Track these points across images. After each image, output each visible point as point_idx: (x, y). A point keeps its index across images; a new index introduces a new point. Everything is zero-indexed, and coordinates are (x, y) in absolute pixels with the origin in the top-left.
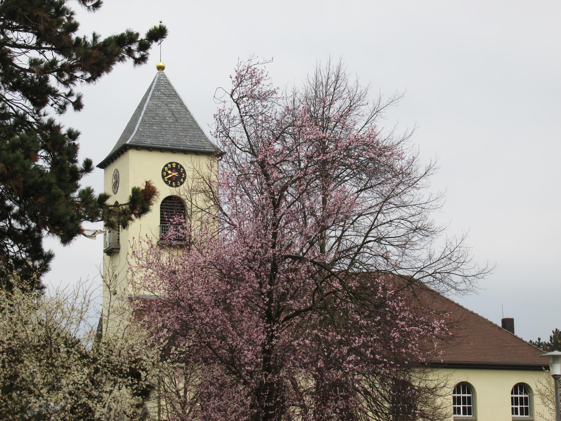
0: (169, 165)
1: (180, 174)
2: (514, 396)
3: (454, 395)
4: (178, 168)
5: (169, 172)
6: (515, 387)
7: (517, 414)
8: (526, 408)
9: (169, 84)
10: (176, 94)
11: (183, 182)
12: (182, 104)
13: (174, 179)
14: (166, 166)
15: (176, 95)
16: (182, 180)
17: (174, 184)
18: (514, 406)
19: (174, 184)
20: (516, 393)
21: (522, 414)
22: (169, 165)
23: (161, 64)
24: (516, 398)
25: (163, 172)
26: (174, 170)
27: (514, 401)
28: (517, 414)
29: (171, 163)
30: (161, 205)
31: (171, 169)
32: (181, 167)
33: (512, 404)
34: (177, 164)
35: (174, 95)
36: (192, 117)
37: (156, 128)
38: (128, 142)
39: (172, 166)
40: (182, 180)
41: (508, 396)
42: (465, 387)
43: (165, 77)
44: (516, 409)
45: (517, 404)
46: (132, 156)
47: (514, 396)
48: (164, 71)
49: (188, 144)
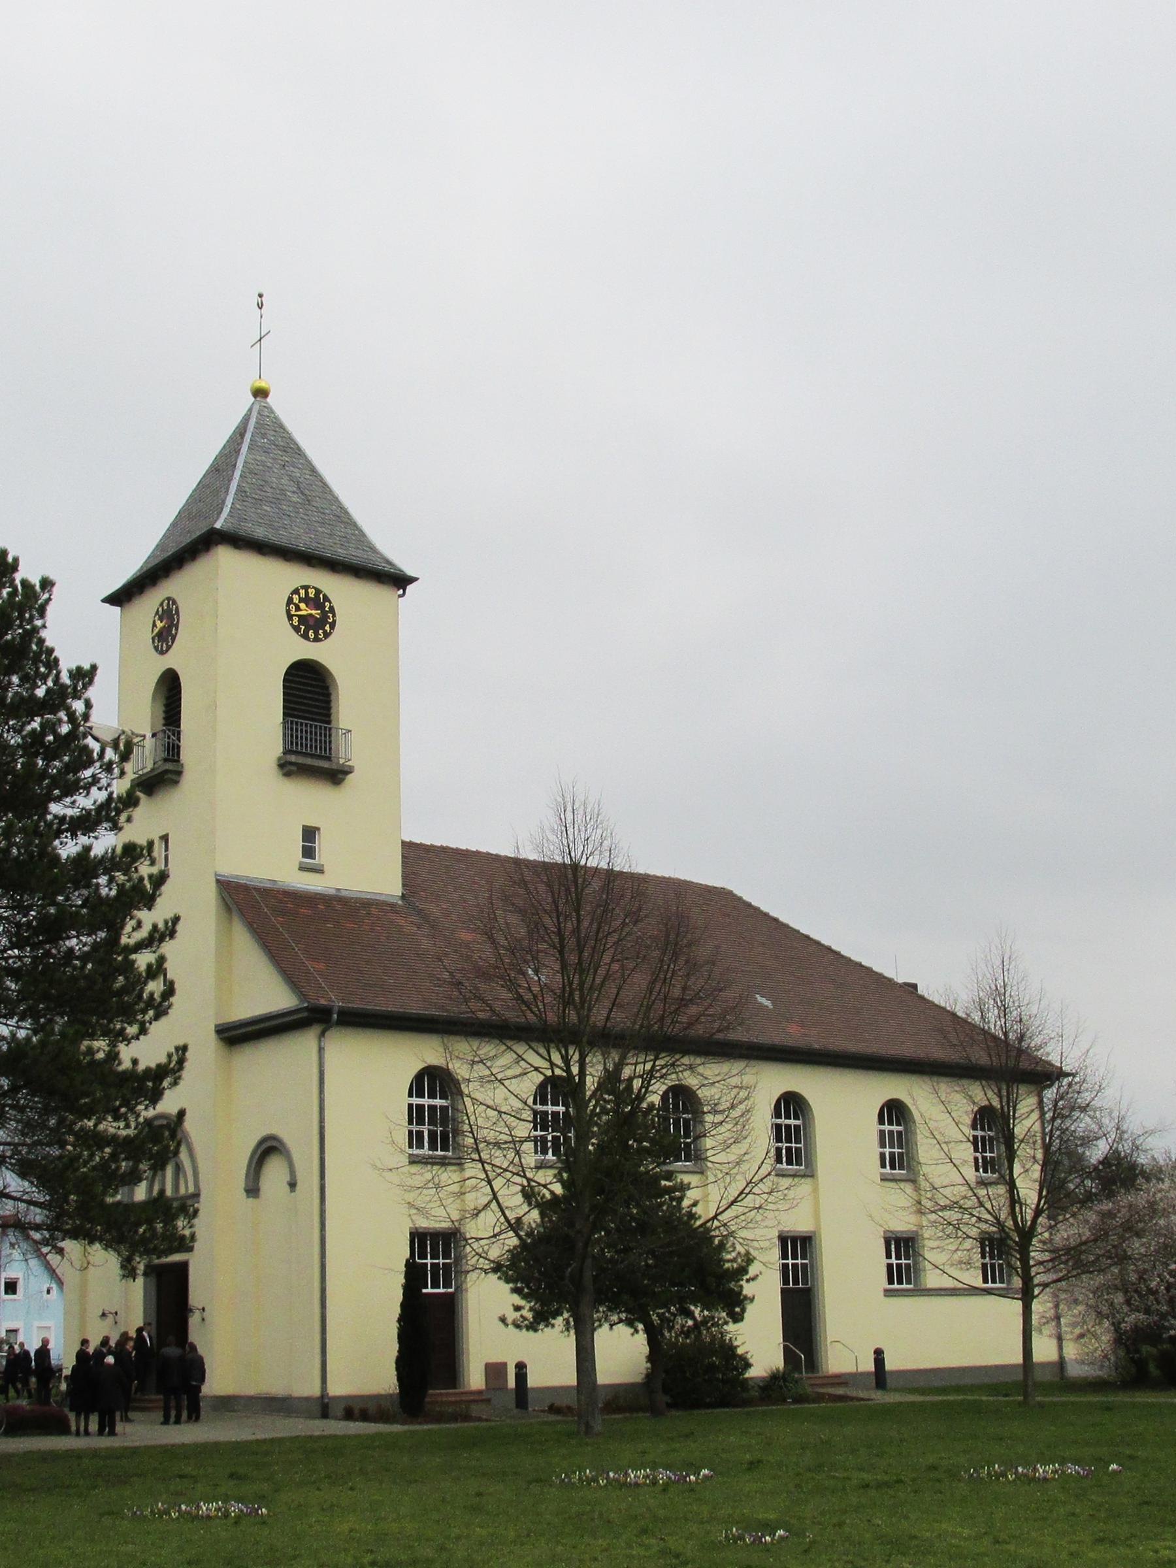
0: (302, 592)
1: (324, 615)
2: (416, 1101)
3: (779, 1121)
4: (318, 600)
5: (303, 606)
6: (419, 1078)
7: (420, 1145)
8: (778, 1139)
9: (281, 426)
10: (299, 449)
11: (331, 633)
12: (314, 471)
13: (311, 622)
14: (296, 591)
15: (298, 452)
16: (327, 628)
17: (311, 634)
18: (415, 1128)
19: (311, 634)
20: (420, 1095)
21: (433, 1147)
22: (302, 592)
23: (263, 384)
24: (420, 1108)
25: (288, 604)
26: (311, 603)
27: (416, 1114)
28: (420, 1145)
29: (306, 588)
30: (286, 674)
31: (306, 600)
32: (326, 598)
33: (410, 1122)
34: (318, 591)
35: (292, 450)
36: (336, 499)
37: (268, 509)
38: (218, 525)
39: (307, 593)
40: (327, 628)
41: (400, 1101)
42: (791, 1104)
43: (272, 412)
44: (420, 1134)
45: (420, 1121)
46: (224, 558)
47: (416, 1101)
48: (269, 400)
49: (342, 553)
